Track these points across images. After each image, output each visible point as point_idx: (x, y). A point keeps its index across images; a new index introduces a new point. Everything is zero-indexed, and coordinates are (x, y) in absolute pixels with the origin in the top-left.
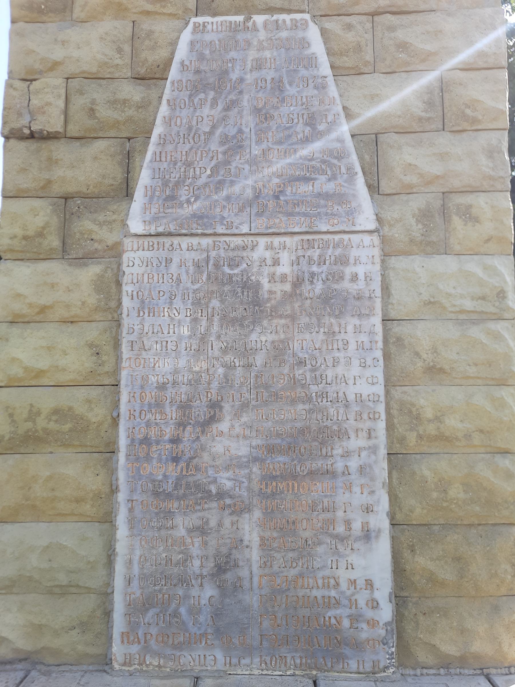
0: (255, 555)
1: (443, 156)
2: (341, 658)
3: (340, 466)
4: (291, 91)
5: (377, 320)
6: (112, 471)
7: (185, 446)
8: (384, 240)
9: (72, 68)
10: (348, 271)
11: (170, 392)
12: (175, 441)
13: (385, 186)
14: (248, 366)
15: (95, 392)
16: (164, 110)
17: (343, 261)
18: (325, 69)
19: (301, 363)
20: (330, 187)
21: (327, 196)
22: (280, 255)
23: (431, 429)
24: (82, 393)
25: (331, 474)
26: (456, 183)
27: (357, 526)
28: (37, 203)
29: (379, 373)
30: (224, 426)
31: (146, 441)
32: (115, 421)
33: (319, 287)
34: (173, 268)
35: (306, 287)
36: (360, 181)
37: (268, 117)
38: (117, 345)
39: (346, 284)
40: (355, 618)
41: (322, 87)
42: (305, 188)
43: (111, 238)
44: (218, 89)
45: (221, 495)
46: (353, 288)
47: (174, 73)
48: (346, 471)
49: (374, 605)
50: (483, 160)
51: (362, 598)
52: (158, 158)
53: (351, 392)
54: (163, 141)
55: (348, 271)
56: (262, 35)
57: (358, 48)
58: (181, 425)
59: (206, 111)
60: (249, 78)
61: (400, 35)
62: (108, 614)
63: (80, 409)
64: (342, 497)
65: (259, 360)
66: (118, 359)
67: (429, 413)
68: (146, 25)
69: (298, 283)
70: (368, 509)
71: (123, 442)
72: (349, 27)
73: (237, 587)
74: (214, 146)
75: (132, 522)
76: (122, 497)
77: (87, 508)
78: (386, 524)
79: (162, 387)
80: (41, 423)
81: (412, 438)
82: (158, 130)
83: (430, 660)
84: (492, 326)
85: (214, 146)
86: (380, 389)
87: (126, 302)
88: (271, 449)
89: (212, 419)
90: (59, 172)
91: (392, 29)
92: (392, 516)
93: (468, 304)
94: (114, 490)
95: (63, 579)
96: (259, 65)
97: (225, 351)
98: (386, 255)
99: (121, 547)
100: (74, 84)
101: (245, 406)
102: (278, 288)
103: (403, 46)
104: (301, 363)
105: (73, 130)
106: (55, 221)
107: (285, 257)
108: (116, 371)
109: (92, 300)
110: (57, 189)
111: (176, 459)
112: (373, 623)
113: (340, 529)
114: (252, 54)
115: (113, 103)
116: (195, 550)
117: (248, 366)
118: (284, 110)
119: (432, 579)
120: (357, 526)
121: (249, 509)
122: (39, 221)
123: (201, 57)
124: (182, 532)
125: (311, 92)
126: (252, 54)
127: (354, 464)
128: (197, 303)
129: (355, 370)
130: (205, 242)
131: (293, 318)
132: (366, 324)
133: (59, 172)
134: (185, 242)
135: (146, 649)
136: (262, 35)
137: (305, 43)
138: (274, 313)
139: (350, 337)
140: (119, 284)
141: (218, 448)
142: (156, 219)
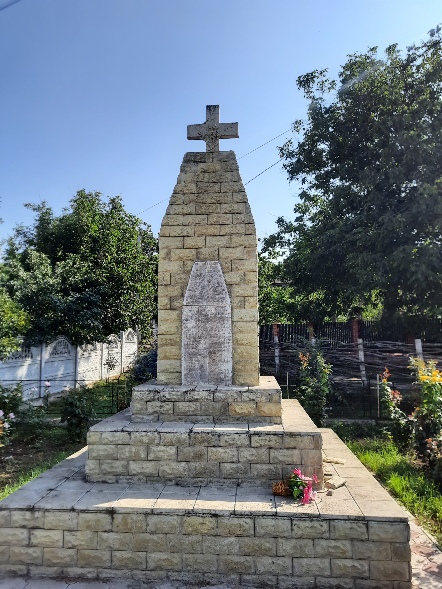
0: (207, 365)
1: (244, 290)
2: (223, 383)
3: (223, 349)
4: (215, 277)
5: (230, 322)
6: (181, 350)
7: (194, 346)
8: (232, 306)
9: (172, 271)
10: (225, 312)
11: (192, 336)
12: (193, 345)
13: (233, 295)
14: (206, 331)
15: (177, 336)
16: (190, 281)
17: (224, 310)
18: (221, 272)
19: (216, 330)
20: (222, 296)
21: (221, 298)
22: (434, 501)
23: (240, 342)
24: (175, 336)
25: (221, 350)
26: (247, 295)
27: (226, 360)
28: (166, 299)
29: (230, 332)
30: (202, 342)
31: (187, 345)
32: (181, 341)
33: (220, 316)
34: (192, 312)
35: (217, 316)
36: (228, 295)
37: (210, 282)
38: (181, 326)
39: (225, 315)
40: (225, 376)
41: (220, 276)
42: (217, 296)
43: (179, 305)
44: (200, 277)
45: (201, 355)
46: (226, 316)
47: (192, 273)
48: (224, 350)
49: (229, 374)
50: (252, 291)
51: (226, 372)
52: (189, 290)
53: (225, 335)
54: (190, 287)
55: (225, 312)
56: (209, 266)
57: (228, 268)
58: (194, 342)
59: (198, 281)
60: (207, 274)
61: (236, 265)
62: (181, 376)
63: (175, 339)
64: (223, 355)
65: (208, 329)
66: (182, 329)
67: (240, 339)
68: (186, 262)
69: (216, 315)
70: (228, 357)
71: (183, 345)
72: (226, 263)
73: (204, 371)
74: (200, 288)
75: (185, 360)
76: (183, 355)
77: (177, 357)
78: (231, 359)
79: (190, 335)
80: (168, 341)
81: (237, 344)
82: (189, 285)
83: (239, 384)
84: (253, 323)
85: (200, 288)
86: (231, 335)
87: (183, 318)
88: (210, 346)
89: (200, 341)
90: (170, 293)
91: (235, 263)
92: (232, 358)
93: (248, 319)
94: (182, 354)
95: (173, 370)
96: (208, 272)
97: (386, 174)
98: (232, 310)
99: (183, 364)
100: (172, 274)
101: (206, 338)
102: (212, 316)
103: (237, 268)
104: (216, 330)
105: (172, 284)
106: (169, 302)
107: (213, 310)
108: (181, 331)
109: (177, 318)
110: (169, 296)
111: (193, 348)
112: (228, 377)
113: (223, 360)
114: (207, 270)
115: (180, 278)
116: (197, 364)
117: (206, 331)
118: (213, 281)
119: (239, 369)
120: (226, 360)
121: (206, 357)
122: (166, 302)
123: (197, 270)
124: (194, 361)
125: (218, 277)
126: (207, 270)
127: (226, 349)
128: (196, 318)
129: (226, 331)
130: (198, 307)
131: (215, 321)
132: (229, 322)
133: (170, 293)
134: (194, 307)
135: (188, 381)
136: (209, 266)
137: (217, 267)
138: (211, 320)
139: (225, 325)
140: (181, 315)
141: (201, 346)
142: (189, 303)
